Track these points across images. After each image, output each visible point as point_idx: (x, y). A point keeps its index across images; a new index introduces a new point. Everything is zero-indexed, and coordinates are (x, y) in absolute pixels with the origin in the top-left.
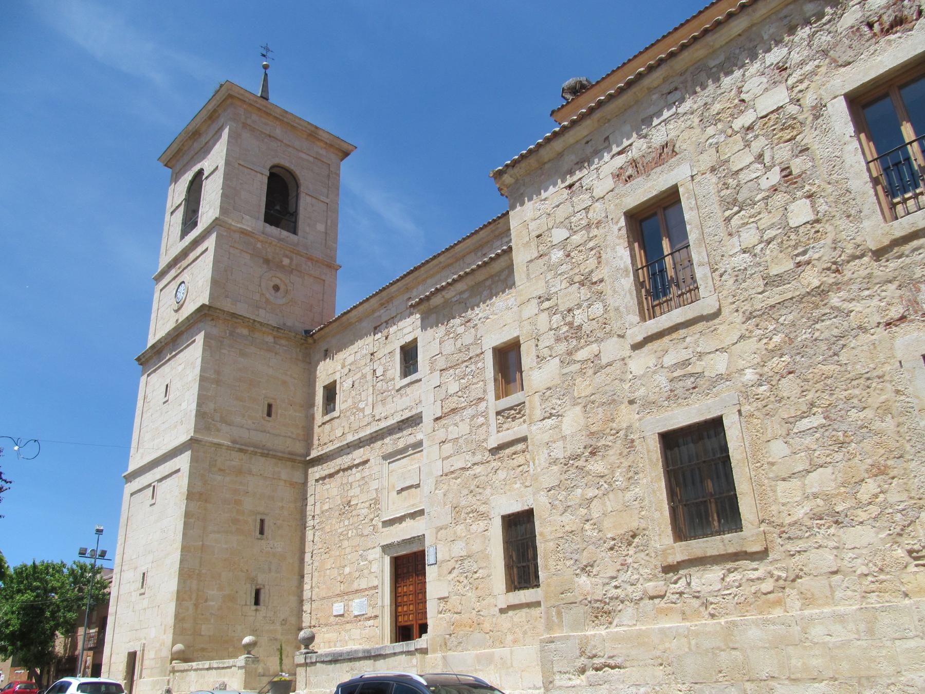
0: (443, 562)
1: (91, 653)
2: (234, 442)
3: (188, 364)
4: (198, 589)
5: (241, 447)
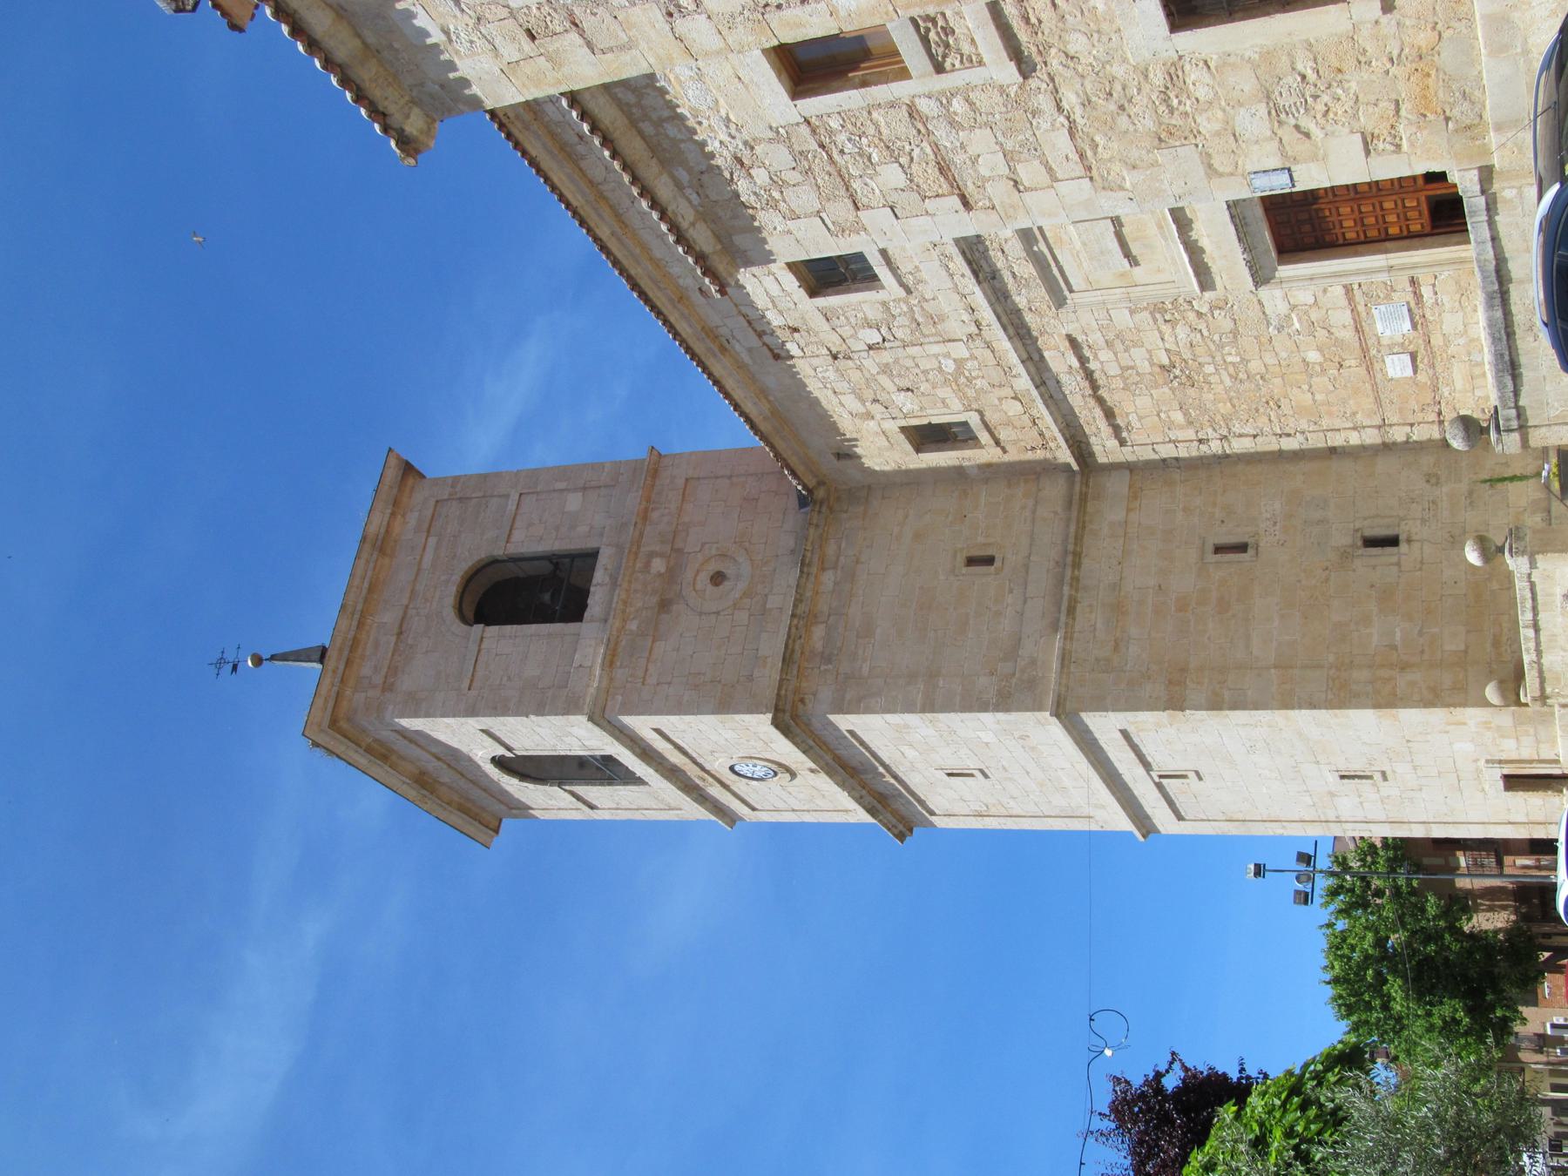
0: (1284, 155)
1: (1508, 860)
2: (1055, 627)
3: (901, 740)
4: (1370, 667)
5: (1064, 611)
